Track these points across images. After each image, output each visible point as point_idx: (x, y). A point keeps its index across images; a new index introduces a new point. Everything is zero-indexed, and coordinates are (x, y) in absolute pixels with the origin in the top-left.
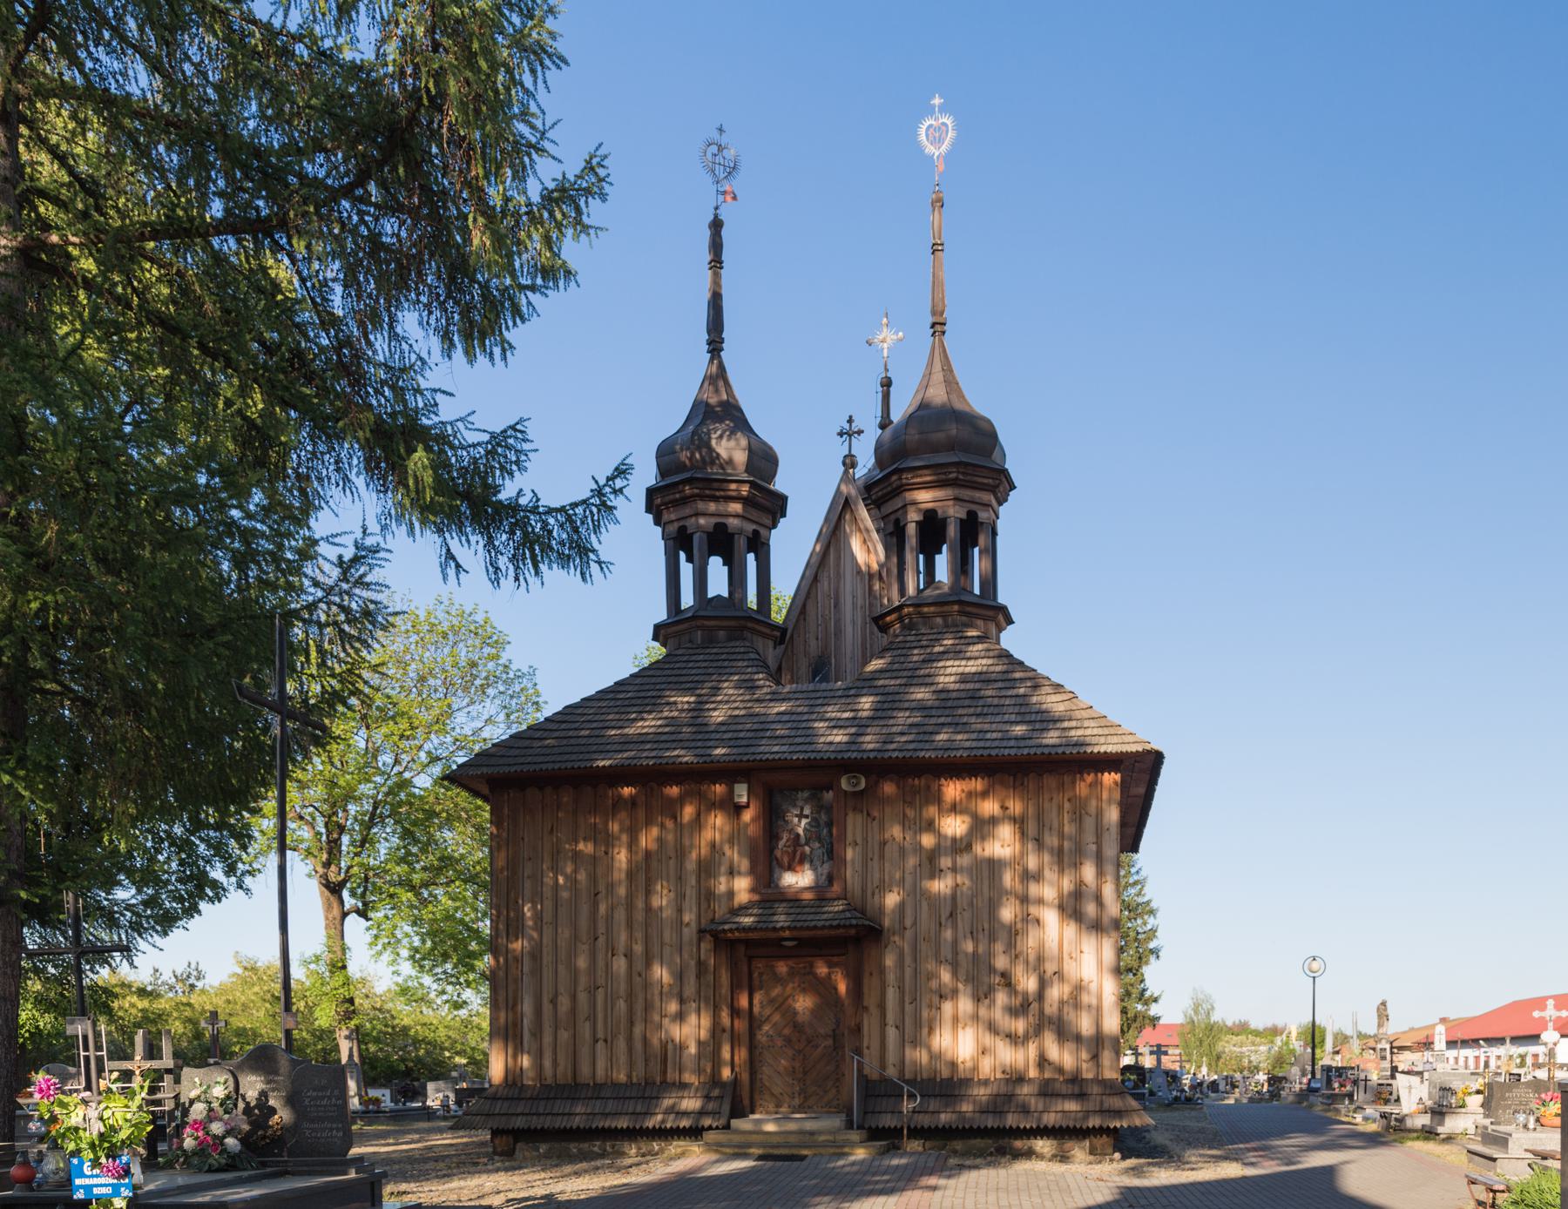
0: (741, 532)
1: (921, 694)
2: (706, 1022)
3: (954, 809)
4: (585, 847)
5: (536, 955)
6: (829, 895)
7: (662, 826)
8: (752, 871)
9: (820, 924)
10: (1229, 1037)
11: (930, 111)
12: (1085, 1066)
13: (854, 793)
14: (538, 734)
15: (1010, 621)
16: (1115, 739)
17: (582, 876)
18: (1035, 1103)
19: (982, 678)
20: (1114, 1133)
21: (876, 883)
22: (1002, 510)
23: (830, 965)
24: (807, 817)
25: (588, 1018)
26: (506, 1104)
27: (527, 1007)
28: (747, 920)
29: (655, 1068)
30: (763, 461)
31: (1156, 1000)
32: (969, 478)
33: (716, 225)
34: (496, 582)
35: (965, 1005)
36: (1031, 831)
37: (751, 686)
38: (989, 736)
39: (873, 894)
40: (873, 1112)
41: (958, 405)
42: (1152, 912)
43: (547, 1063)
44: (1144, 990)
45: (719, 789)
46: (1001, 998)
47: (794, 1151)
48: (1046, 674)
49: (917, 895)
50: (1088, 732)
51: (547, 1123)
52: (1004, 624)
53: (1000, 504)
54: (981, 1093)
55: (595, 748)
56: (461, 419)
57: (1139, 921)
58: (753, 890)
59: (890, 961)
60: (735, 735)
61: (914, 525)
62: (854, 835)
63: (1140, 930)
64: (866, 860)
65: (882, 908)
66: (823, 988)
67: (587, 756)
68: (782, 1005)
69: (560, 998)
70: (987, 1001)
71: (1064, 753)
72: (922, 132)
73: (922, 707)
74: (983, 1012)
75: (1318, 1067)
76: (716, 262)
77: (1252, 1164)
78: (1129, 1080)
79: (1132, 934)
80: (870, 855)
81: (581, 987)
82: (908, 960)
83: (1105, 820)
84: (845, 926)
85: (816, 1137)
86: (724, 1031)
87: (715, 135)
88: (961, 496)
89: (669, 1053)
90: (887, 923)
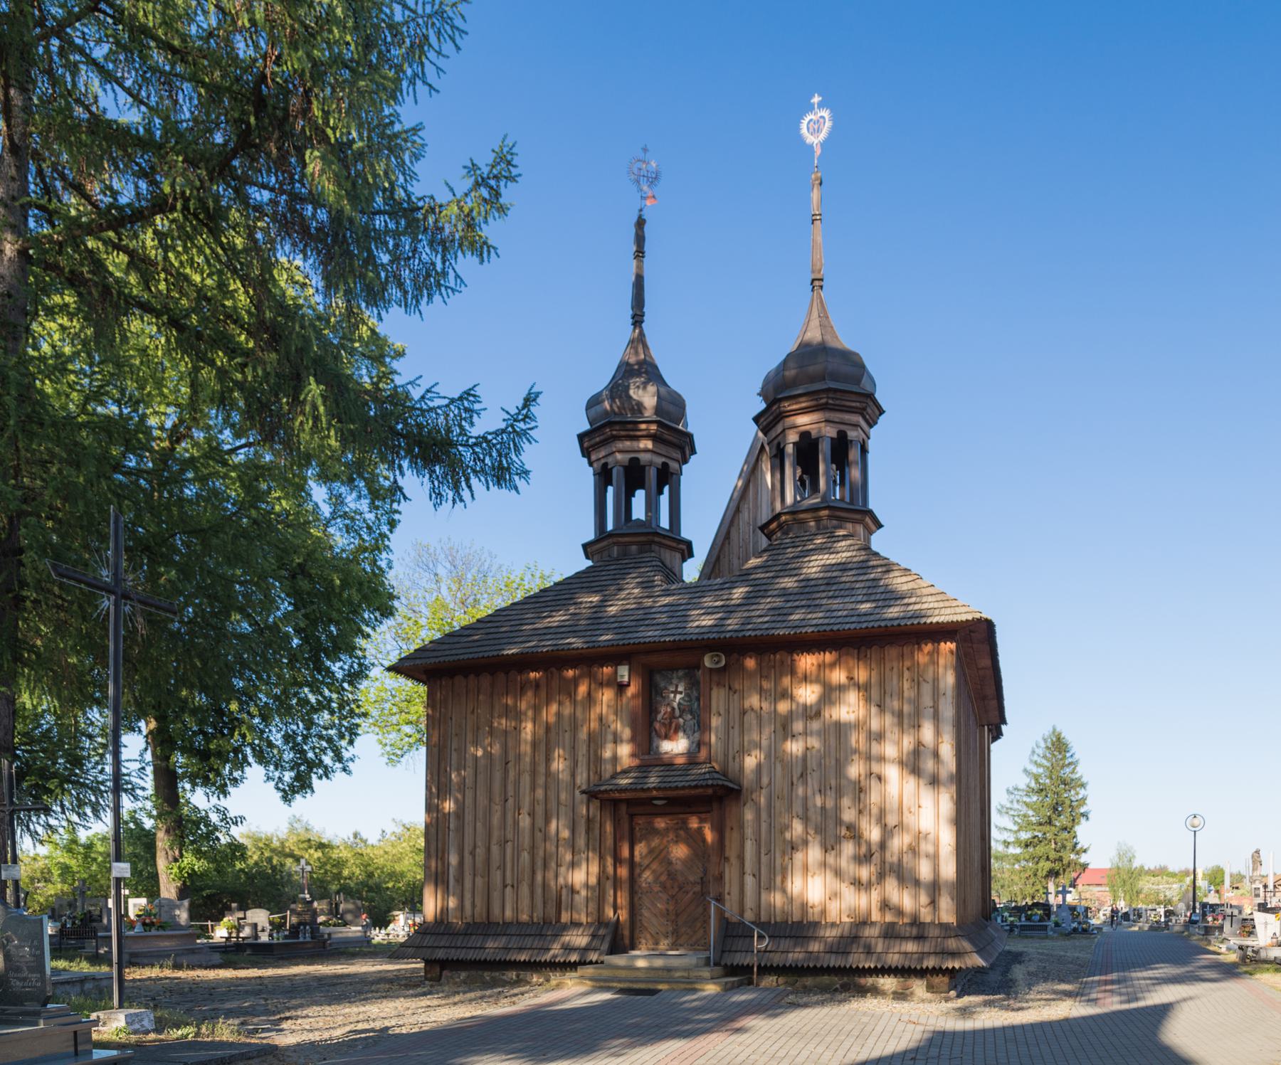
0: (651, 464)
1: (788, 583)
2: (595, 869)
3: (806, 679)
4: (503, 723)
5: (460, 814)
7: (560, 704)
8: (633, 740)
9: (681, 785)
10: (1148, 878)
11: (810, 108)
12: (922, 910)
15: (880, 526)
16: (948, 611)
19: (843, 567)
20: (951, 972)
21: (737, 747)
23: (702, 821)
24: (681, 693)
25: (498, 868)
27: (453, 860)
28: (624, 782)
29: (552, 911)
30: (672, 407)
31: (1085, 851)
32: (838, 402)
33: (640, 223)
35: (814, 853)
36: (877, 696)
37: (647, 585)
38: (835, 614)
39: (734, 758)
40: (730, 951)
41: (832, 343)
42: (1083, 786)
44: (1076, 844)
45: (607, 670)
46: (848, 848)
47: (651, 986)
49: (775, 755)
50: (925, 606)
51: (461, 954)
52: (873, 527)
53: (871, 426)
54: (830, 934)
55: (506, 641)
56: (410, 383)
57: (1073, 792)
58: (633, 755)
59: (749, 816)
60: (621, 625)
61: (791, 445)
62: (718, 706)
63: (1073, 799)
64: (728, 727)
65: (742, 768)
66: (695, 839)
68: (660, 856)
70: (833, 853)
71: (899, 625)
72: (804, 130)
73: (785, 593)
75: (1197, 905)
76: (640, 253)
77: (1095, 1000)
78: (1036, 914)
79: (1068, 802)
80: (731, 725)
81: (494, 840)
82: (764, 816)
83: (942, 685)
84: (702, 786)
86: (608, 878)
87: (641, 155)
88: (831, 419)
89: (561, 898)
90: (746, 783)
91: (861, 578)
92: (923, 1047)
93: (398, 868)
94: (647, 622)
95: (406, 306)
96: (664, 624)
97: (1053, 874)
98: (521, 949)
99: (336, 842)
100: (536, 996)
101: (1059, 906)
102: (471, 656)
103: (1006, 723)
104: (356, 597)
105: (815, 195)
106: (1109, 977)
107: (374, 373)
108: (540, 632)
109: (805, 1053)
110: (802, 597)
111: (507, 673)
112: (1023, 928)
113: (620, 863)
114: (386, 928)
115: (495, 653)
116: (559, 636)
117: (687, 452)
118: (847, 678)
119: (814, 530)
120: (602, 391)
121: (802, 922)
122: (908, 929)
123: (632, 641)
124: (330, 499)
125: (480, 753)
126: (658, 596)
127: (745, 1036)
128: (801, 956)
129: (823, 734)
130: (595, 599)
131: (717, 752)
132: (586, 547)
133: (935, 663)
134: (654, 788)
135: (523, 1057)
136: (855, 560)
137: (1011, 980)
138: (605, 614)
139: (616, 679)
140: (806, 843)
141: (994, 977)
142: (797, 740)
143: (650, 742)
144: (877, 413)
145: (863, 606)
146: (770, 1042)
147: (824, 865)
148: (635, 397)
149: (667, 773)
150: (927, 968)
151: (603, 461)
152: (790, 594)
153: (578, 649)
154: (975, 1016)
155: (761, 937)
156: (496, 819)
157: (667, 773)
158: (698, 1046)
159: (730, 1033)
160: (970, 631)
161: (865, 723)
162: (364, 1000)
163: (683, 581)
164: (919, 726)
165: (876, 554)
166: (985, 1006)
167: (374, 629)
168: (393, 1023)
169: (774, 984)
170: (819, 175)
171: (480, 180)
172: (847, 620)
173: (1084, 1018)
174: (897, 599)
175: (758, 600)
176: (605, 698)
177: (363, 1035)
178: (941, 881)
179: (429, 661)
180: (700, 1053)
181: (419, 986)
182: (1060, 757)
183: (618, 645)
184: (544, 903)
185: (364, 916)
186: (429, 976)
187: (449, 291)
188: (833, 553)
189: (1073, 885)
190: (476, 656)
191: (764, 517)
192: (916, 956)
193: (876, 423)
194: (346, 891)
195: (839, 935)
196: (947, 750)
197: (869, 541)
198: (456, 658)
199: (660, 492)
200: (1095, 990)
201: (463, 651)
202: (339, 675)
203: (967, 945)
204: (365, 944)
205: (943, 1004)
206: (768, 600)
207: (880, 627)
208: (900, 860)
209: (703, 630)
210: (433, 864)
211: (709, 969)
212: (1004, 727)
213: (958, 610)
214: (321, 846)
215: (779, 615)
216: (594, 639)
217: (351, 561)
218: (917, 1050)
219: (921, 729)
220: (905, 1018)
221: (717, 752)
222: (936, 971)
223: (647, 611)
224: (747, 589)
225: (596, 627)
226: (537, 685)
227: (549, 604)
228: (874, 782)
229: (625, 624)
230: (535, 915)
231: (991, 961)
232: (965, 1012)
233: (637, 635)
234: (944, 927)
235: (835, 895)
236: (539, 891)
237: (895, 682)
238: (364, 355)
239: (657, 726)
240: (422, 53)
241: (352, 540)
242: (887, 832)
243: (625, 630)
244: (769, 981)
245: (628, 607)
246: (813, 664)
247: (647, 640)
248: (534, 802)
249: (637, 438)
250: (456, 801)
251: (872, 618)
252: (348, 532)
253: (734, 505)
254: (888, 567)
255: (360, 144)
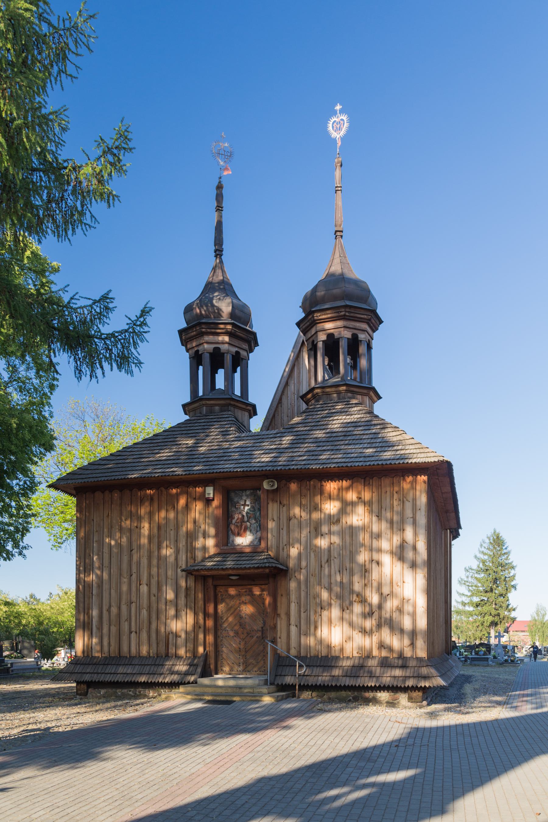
0: (228, 352)
1: (319, 434)
3: (330, 498)
6: (259, 550)
8: (216, 536)
9: (248, 566)
11: (334, 113)
13: (273, 491)
14: (104, 462)
15: (379, 398)
16: (422, 455)
17: (124, 540)
18: (378, 671)
19: (355, 424)
20: (424, 689)
21: (285, 543)
22: (375, 335)
24: (248, 505)
26: (82, 667)
27: (95, 613)
31: (514, 610)
33: (220, 187)
34: (79, 378)
35: (335, 612)
37: (225, 434)
38: (349, 456)
40: (280, 675)
41: (349, 275)
42: (513, 568)
43: (105, 643)
44: (509, 605)
45: (199, 490)
46: (357, 608)
47: (228, 698)
48: (389, 422)
49: (310, 548)
50: (408, 452)
51: (102, 678)
52: (375, 399)
53: (374, 331)
54: (346, 663)
55: (130, 468)
57: (507, 571)
58: (217, 545)
61: (321, 342)
64: (279, 529)
65: (288, 556)
66: (257, 602)
67: (125, 473)
69: (112, 608)
72: (330, 125)
73: (317, 441)
74: (346, 616)
76: (219, 208)
77: (516, 707)
80: (281, 527)
81: (124, 601)
82: (303, 587)
84: (262, 567)
85: (243, 690)
88: (348, 326)
91: (367, 432)
92: (404, 738)
93: (60, 618)
94: (225, 458)
95: (58, 236)
96: (236, 460)
97: (494, 624)
98: (141, 674)
99: (19, 601)
100: (152, 706)
101: (496, 646)
102: (106, 479)
103: (461, 528)
104: (28, 436)
105: (338, 173)
106: (526, 692)
107: (38, 283)
108: (153, 463)
109: (328, 742)
110: (328, 444)
111: (131, 490)
112: (473, 659)
113: (208, 617)
114: (52, 659)
115: (123, 477)
116: (166, 466)
117: (253, 345)
118: (357, 497)
119: (336, 400)
120: (193, 302)
121: (328, 656)
122: (396, 661)
123: (215, 471)
124: (8, 368)
125: (113, 543)
126: (233, 441)
127: (289, 731)
128: (327, 678)
129: (342, 533)
130: (190, 442)
131: (272, 545)
132: (184, 406)
133: (413, 488)
134: (230, 568)
135: (141, 747)
136: (363, 420)
137: (463, 694)
138: (198, 452)
139: (205, 495)
140: (330, 605)
141: (453, 692)
142: (325, 538)
143: (228, 537)
144: (378, 323)
145: (368, 451)
146: (305, 735)
147: (342, 619)
148: (216, 304)
149: (239, 558)
150: (408, 686)
151: (196, 349)
152: (320, 442)
153: (179, 475)
154: (438, 718)
155: (301, 666)
156: (125, 588)
157: (239, 558)
158: (258, 738)
159: (279, 729)
160: (437, 469)
161: (369, 527)
162: (34, 709)
163: (250, 431)
164: (403, 530)
165: (377, 416)
166: (445, 711)
167: (40, 459)
168: (53, 725)
169: (310, 697)
170: (340, 159)
171: (106, 149)
172: (357, 460)
173: (508, 719)
174: (389, 446)
175: (299, 445)
176: (197, 508)
177: (32, 733)
178: (417, 630)
179: (77, 481)
180: (259, 743)
181: (73, 699)
182: (498, 549)
183: (206, 473)
184: (157, 644)
185: (36, 651)
186: (79, 692)
187: (87, 226)
188: (348, 415)
189: (507, 631)
190: (109, 478)
191: (304, 389)
192: (401, 678)
193: (377, 329)
194: (23, 633)
195: (351, 665)
196: (422, 546)
197: (372, 407)
198: (96, 479)
199: (235, 371)
200: (516, 701)
201: (101, 475)
202: (16, 488)
203: (433, 671)
204: (37, 670)
205: (418, 710)
206: (306, 445)
207: (378, 464)
208: (391, 617)
209: (262, 465)
210: (82, 617)
211: (267, 687)
212: (460, 530)
213: (429, 455)
214: (7, 604)
215: (313, 455)
216: (190, 469)
217: (24, 411)
218: (400, 740)
219: (405, 531)
220: (393, 719)
221: (272, 545)
222: (414, 688)
223: (225, 451)
224: (291, 438)
225: (191, 461)
226: (152, 499)
227: (160, 444)
228: (374, 565)
229: (211, 459)
230: (151, 651)
231: (449, 682)
232: (432, 715)
233: (219, 467)
234: (420, 660)
235: (350, 639)
236: (154, 635)
237: (388, 500)
238: (30, 269)
239: (233, 527)
240: (65, 57)
241: (24, 397)
242: (383, 598)
243: (211, 463)
244: (306, 695)
245: (213, 447)
246: (335, 488)
247: (225, 470)
248: (150, 575)
249: (218, 334)
250: (97, 576)
251: (373, 459)
252: (21, 391)
253: (284, 380)
254: (384, 425)
255: (19, 122)
